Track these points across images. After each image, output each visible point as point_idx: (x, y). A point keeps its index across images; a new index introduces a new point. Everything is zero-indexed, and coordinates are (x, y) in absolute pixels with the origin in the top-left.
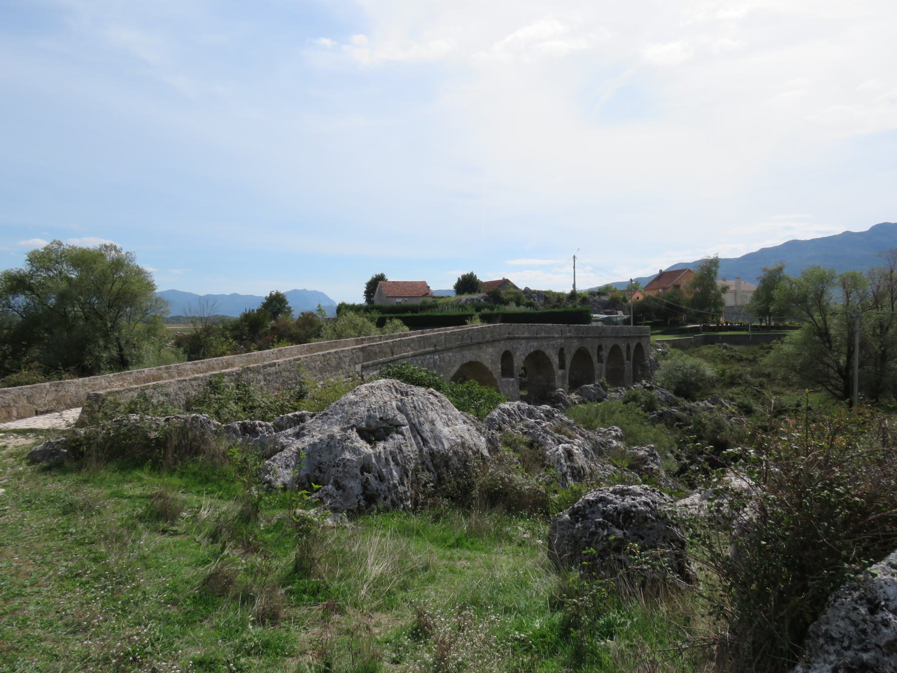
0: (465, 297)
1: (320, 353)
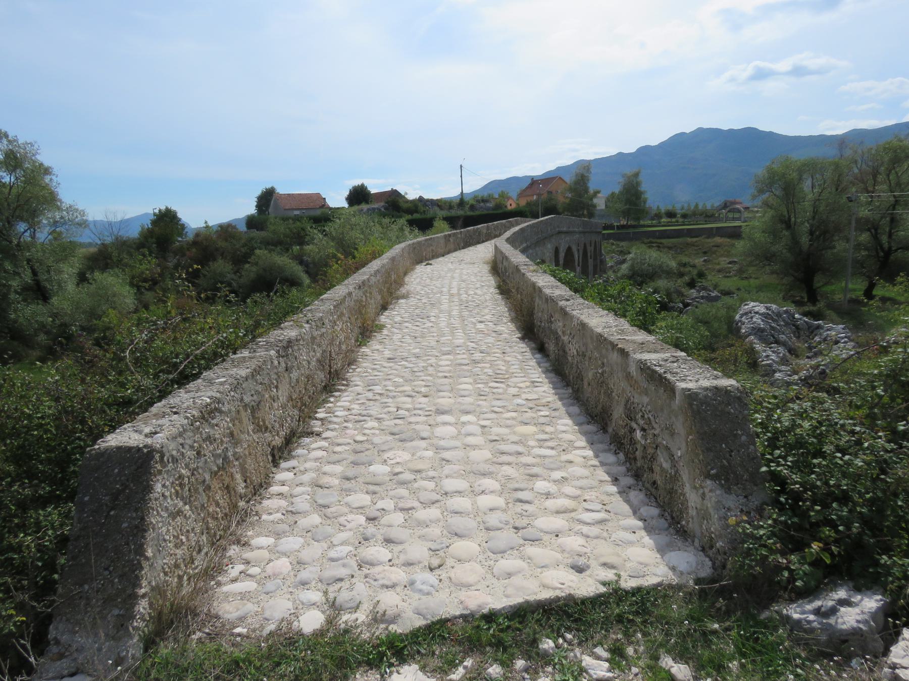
1: (375, 265)
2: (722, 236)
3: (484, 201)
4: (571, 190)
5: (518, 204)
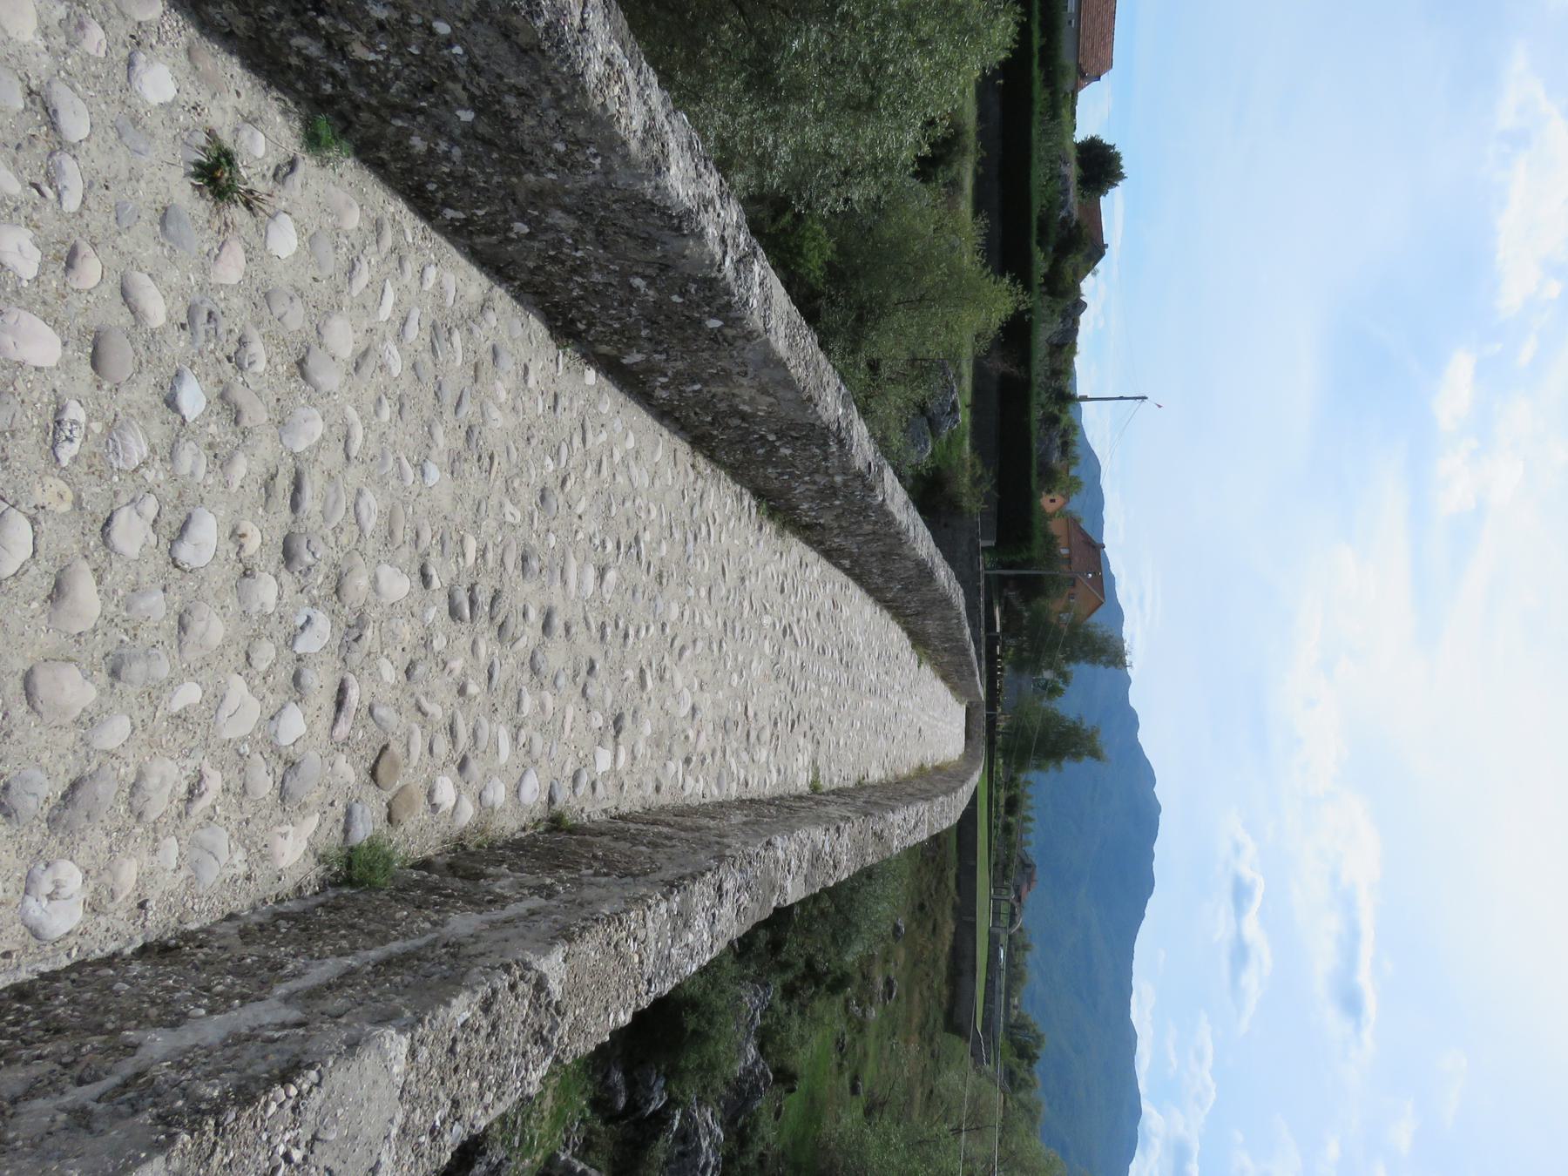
0: (1072, 171)
2: (955, 934)
3: (1065, 446)
4: (1074, 626)
5: (1052, 515)
